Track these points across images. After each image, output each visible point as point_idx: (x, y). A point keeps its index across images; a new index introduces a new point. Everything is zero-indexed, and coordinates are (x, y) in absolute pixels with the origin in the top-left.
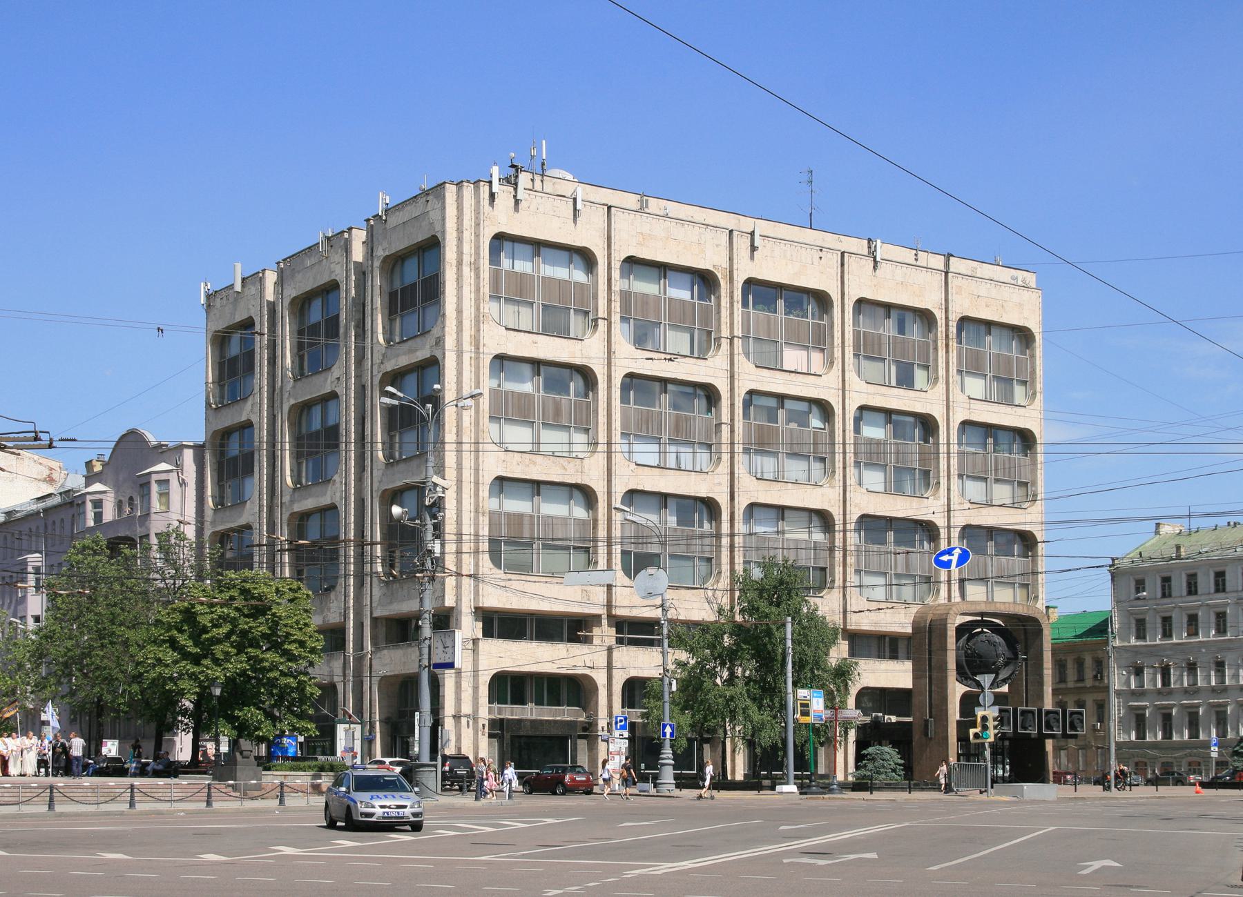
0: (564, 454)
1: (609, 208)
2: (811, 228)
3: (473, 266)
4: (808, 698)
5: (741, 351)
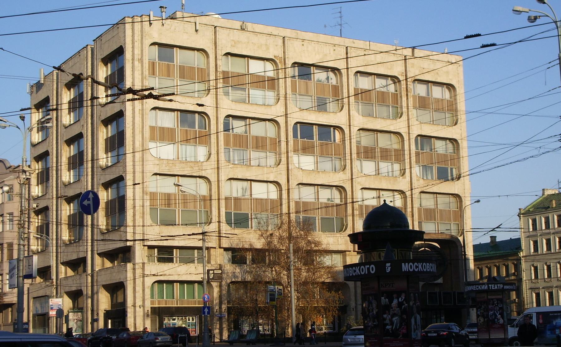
1: (215, 27)
2: (341, 37)
3: (140, 61)
4: (274, 290)
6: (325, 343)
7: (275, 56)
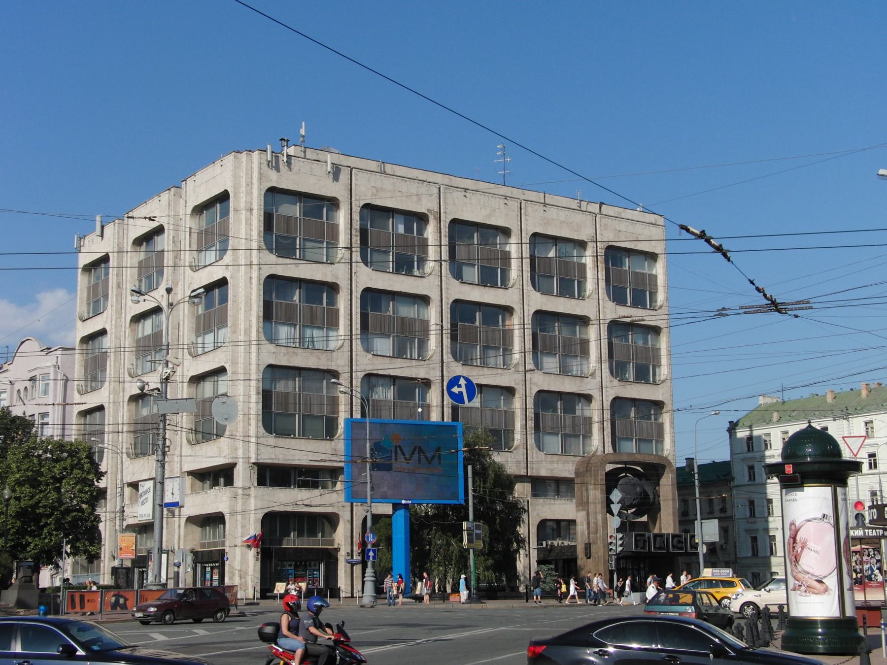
0: (284, 344)
4: (472, 528)
5: (359, 259)
6: (527, 601)
7: (428, 210)
